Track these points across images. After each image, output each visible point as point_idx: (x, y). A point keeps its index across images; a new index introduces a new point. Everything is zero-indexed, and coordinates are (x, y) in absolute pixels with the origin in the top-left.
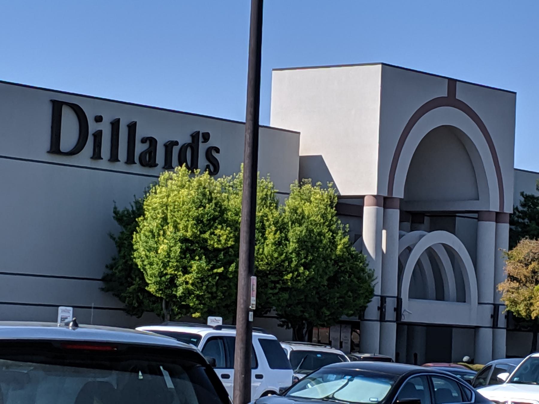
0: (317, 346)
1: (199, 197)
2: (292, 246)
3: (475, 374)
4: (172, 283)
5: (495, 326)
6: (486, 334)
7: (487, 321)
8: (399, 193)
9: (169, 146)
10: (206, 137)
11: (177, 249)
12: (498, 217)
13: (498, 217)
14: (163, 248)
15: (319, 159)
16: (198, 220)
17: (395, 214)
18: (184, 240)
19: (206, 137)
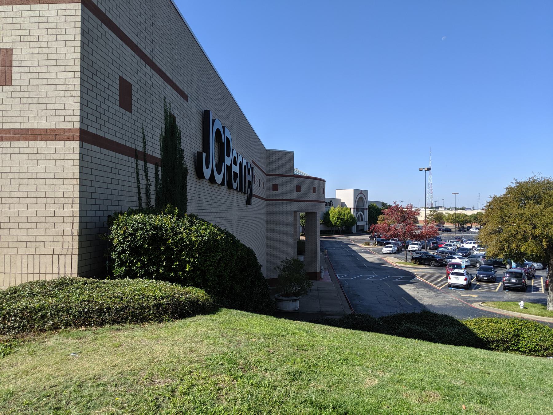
0: (501, 269)
1: (346, 216)
2: (349, 217)
3: (145, 166)
4: (336, 223)
5: (367, 224)
6: (366, 226)
7: (366, 224)
8: (356, 207)
9: (328, 203)
10: (332, 201)
11: (337, 219)
12: (367, 209)
13: (367, 209)
14: (335, 219)
15: (344, 203)
16: (339, 215)
17: (355, 210)
18: (337, 217)
19: (332, 201)
